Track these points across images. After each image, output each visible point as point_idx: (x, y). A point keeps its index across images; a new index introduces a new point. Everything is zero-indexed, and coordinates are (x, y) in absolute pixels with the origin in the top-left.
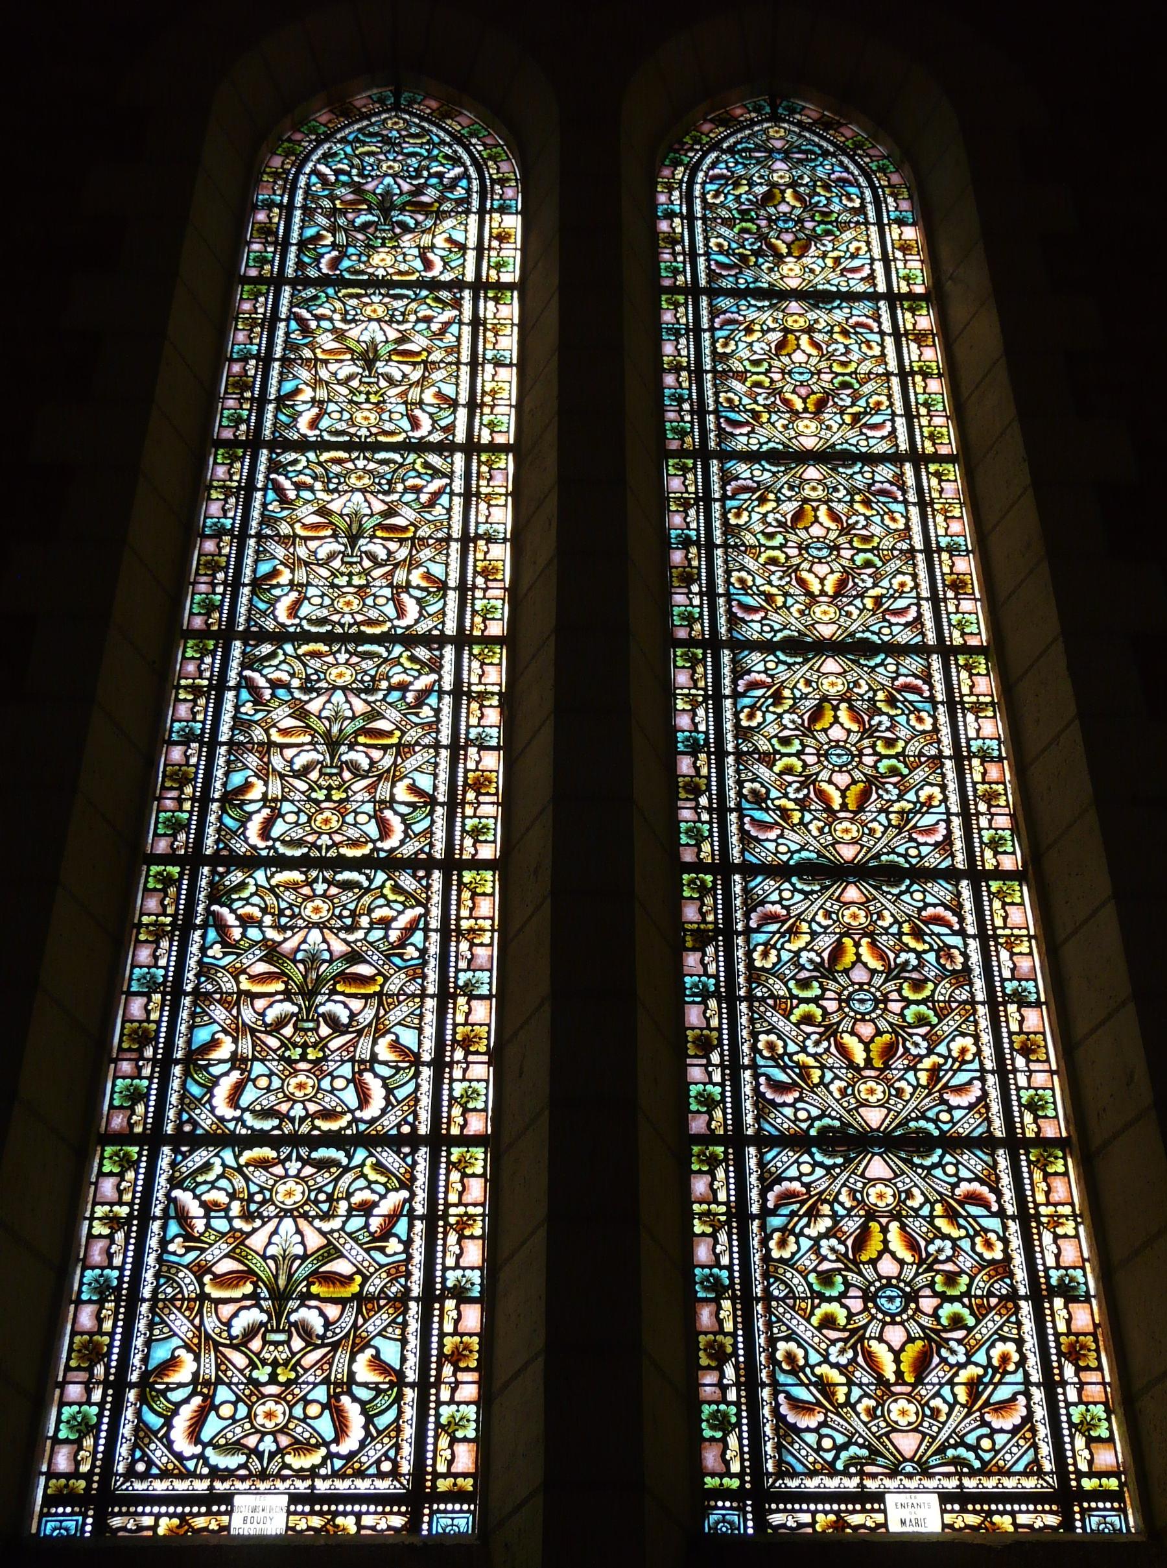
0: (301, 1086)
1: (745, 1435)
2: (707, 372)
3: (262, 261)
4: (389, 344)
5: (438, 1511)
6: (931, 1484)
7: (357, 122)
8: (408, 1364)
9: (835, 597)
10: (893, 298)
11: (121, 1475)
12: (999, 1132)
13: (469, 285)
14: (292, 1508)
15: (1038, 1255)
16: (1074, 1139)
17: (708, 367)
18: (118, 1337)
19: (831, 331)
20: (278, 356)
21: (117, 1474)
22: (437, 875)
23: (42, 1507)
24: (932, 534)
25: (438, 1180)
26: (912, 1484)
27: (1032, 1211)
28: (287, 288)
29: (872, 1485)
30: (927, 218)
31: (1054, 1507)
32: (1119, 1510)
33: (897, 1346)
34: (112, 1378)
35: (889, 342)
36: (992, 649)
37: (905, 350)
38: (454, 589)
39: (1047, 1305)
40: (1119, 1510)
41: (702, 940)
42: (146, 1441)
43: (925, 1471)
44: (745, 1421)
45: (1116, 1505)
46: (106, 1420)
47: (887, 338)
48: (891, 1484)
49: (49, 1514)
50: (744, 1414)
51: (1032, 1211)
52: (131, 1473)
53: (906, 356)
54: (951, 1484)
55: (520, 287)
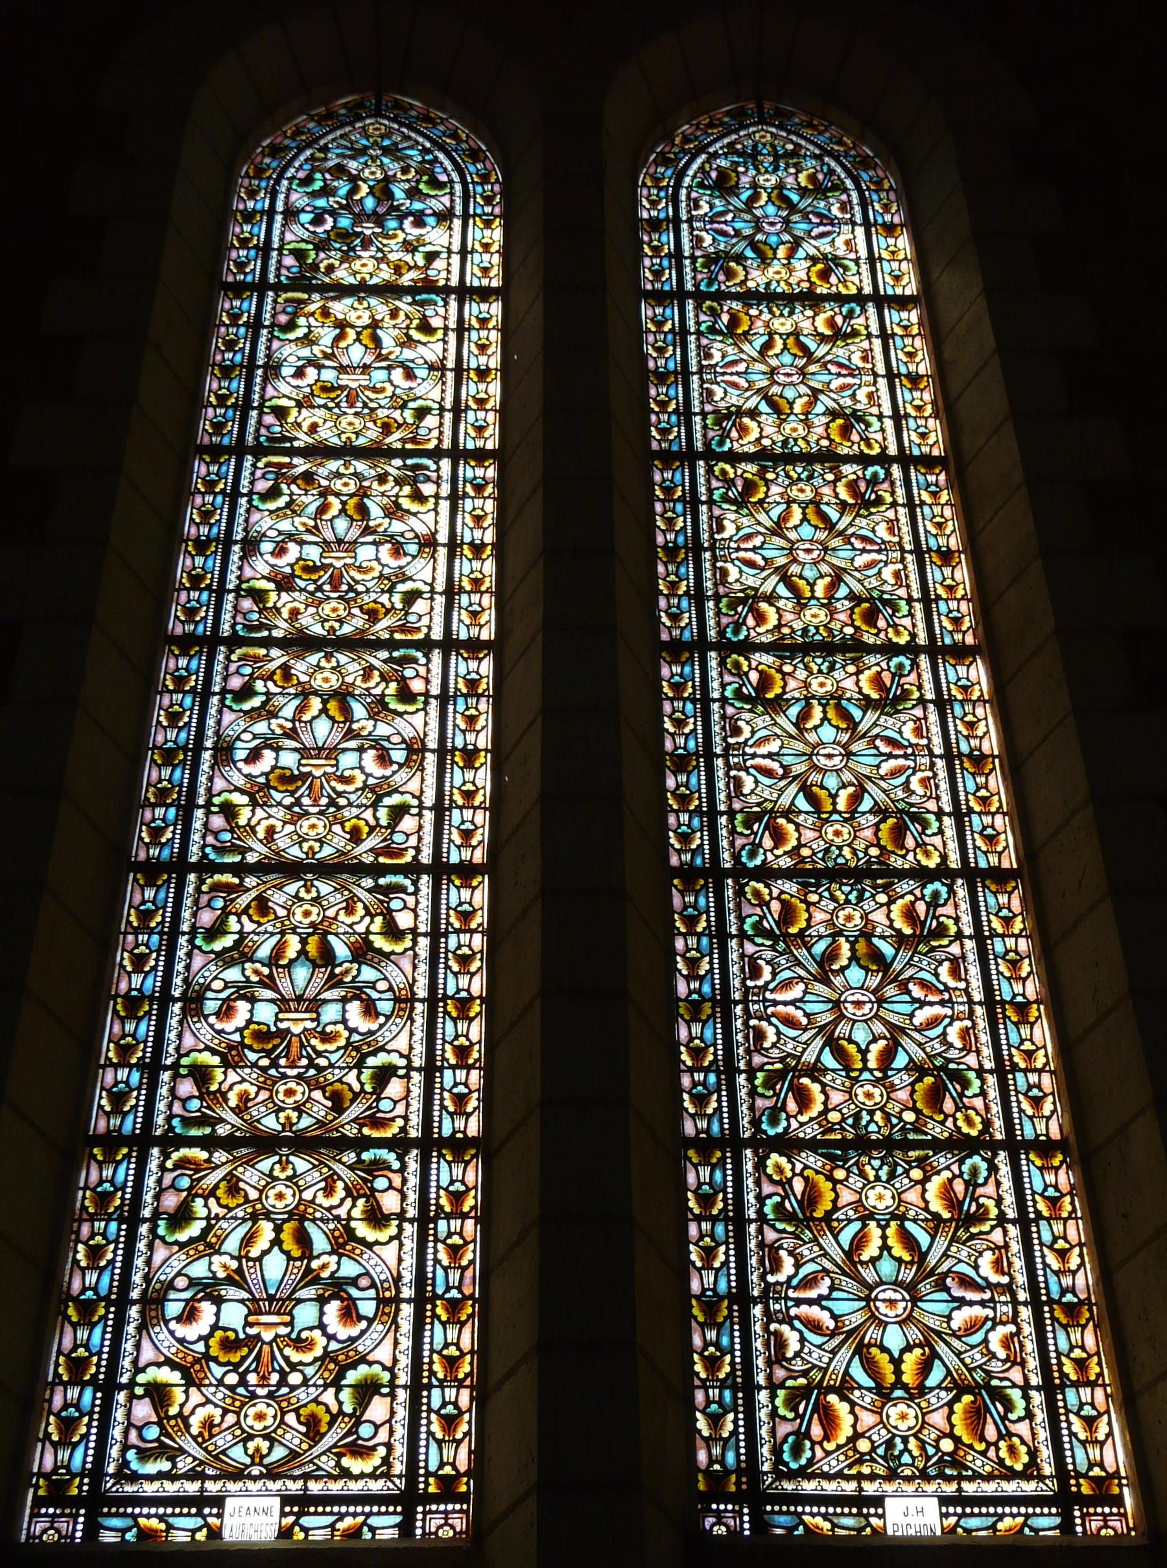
0: (290, 1093)
1: (742, 1444)
2: (696, 414)
3: (218, 427)
4: (371, 336)
5: (430, 1512)
6: (930, 1488)
7: (339, 128)
8: (404, 1265)
9: (888, 1182)
10: (935, 650)
11: (111, 1476)
12: (868, 290)
13: (415, 1143)
14: (287, 1509)
15: (1026, 1180)
16: (1072, 1139)
17: (697, 410)
18: (105, 1356)
19: (816, 331)
20: (260, 363)
21: (107, 1474)
22: (425, 879)
23: (32, 1508)
24: (943, 681)
25: (426, 1260)
26: (909, 1488)
27: (1057, 1381)
28: (271, 293)
29: (870, 1488)
30: (916, 228)
31: (1054, 1510)
32: (1119, 1514)
33: (791, 399)
34: (89, 1466)
35: (882, 383)
36: (951, 460)
37: (942, 673)
38: (446, 498)
39: (1034, 1229)
40: (1119, 1514)
41: (682, 764)
42: (155, 1321)
43: (924, 1476)
44: (742, 1430)
45: (1115, 1510)
46: (94, 1431)
47: (880, 380)
48: (889, 1488)
49: (40, 1515)
50: (741, 1423)
51: (1057, 1381)
52: (119, 1476)
53: (943, 677)
54: (950, 1489)
55: (489, 868)
